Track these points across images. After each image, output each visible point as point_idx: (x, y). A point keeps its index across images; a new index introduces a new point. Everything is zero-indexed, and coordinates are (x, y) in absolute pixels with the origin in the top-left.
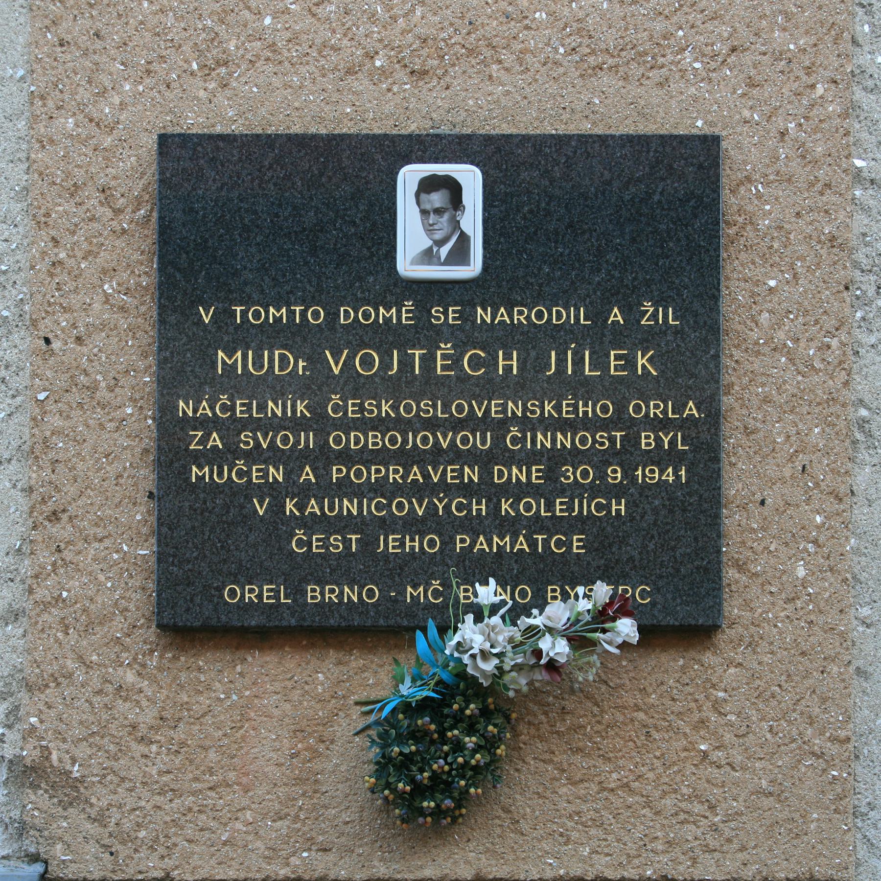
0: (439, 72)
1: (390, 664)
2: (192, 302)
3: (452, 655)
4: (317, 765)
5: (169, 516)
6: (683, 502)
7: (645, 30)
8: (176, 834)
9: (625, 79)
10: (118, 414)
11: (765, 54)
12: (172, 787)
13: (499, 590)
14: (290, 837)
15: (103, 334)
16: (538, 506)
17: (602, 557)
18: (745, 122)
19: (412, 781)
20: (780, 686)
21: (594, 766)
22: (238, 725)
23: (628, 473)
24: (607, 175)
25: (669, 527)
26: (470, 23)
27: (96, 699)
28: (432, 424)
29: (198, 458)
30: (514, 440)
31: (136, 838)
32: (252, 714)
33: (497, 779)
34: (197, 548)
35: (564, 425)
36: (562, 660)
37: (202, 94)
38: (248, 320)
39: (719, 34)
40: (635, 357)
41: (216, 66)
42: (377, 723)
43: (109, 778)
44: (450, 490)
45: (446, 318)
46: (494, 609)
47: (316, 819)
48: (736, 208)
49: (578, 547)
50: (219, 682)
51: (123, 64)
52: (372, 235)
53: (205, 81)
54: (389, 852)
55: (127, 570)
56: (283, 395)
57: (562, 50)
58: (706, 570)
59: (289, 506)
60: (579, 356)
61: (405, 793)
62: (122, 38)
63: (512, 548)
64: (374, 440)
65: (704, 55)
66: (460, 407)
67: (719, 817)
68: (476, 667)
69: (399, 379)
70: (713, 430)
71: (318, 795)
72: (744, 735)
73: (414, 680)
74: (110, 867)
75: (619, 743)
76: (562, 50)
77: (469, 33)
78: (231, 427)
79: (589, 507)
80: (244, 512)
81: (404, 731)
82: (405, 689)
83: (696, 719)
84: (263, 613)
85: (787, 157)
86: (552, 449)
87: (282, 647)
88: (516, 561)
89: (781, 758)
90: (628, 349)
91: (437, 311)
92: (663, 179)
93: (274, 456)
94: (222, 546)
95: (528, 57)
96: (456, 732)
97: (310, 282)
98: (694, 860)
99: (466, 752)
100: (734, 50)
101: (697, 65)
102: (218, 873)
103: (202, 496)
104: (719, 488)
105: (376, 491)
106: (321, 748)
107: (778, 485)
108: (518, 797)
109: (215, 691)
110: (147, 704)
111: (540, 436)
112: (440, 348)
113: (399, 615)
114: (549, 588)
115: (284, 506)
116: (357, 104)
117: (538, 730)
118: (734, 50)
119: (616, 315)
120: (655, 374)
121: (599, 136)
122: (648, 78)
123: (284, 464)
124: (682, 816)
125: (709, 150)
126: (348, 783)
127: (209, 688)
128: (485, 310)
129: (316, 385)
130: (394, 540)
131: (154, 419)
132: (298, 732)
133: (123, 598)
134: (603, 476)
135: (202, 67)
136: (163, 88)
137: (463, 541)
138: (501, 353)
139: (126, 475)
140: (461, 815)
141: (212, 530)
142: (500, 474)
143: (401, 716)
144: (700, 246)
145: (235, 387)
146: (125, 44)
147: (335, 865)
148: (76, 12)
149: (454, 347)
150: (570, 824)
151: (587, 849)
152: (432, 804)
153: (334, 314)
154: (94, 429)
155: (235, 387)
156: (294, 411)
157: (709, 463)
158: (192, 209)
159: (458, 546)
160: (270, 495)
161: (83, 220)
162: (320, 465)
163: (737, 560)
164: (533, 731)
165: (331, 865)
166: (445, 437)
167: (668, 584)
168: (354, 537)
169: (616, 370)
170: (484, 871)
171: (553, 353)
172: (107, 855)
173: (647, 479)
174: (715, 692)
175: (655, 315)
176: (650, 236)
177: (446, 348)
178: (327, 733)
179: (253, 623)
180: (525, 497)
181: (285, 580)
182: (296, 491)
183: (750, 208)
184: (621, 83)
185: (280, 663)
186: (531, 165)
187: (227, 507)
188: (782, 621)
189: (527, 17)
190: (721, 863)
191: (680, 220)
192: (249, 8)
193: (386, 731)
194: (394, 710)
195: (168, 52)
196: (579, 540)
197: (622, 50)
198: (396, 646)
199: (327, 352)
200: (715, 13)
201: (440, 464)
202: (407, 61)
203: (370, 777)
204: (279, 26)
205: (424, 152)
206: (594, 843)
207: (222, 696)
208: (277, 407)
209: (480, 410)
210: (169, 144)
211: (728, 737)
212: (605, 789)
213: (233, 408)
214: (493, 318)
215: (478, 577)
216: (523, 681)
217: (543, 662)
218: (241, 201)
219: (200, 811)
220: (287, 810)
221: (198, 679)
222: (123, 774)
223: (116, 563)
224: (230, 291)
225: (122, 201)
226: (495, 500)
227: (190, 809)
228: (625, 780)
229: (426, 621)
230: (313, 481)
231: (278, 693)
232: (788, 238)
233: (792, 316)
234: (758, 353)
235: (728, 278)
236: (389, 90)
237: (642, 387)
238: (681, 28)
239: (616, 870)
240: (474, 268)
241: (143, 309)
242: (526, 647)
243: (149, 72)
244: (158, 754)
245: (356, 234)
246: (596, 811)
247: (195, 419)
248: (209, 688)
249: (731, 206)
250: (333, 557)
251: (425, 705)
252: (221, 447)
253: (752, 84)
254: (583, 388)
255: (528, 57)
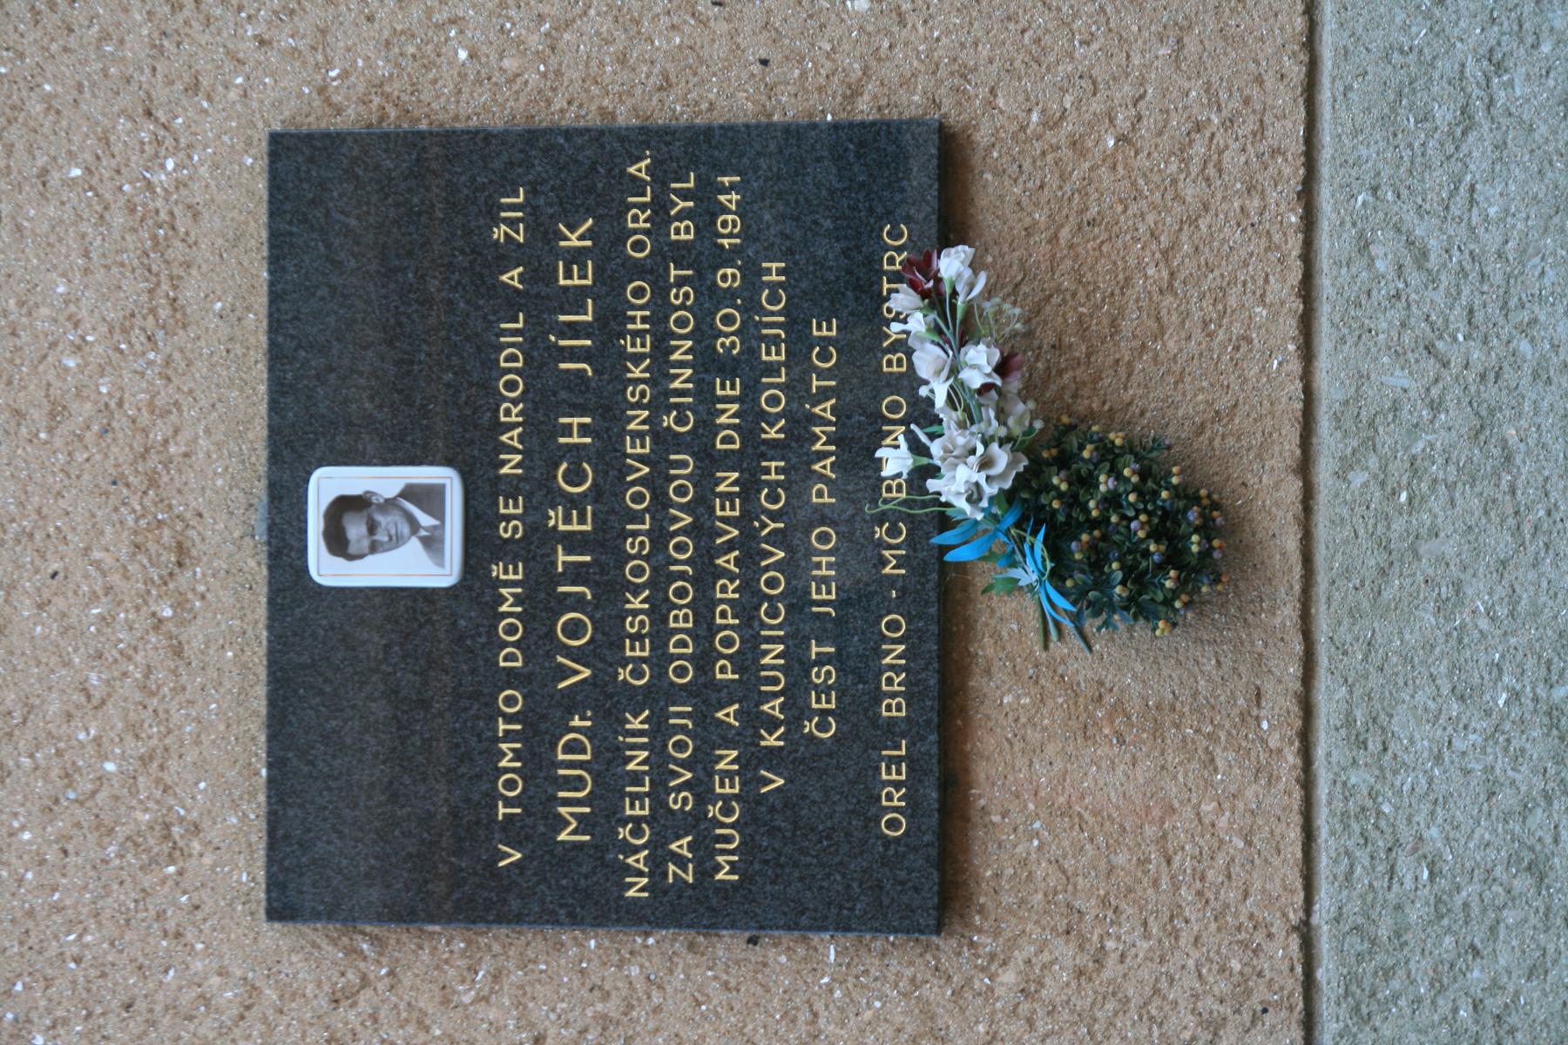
0: (179, 526)
1: (990, 599)
2: (493, 875)
3: (983, 510)
4: (1134, 707)
5: (785, 914)
6: (767, 179)
7: (123, 238)
8: (1236, 915)
9: (188, 265)
10: (640, 986)
11: (154, 69)
12: (1166, 919)
13: (888, 441)
14: (1240, 747)
15: (531, 1005)
16: (772, 386)
17: (844, 295)
18: (245, 95)
19: (1161, 568)
20: (1023, 32)
21: (1137, 300)
22: (1076, 820)
23: (726, 258)
24: (323, 292)
25: (801, 199)
26: (114, 483)
27: (1042, 1026)
28: (659, 537)
29: (706, 870)
30: (681, 421)
31: (1241, 973)
32: (1062, 799)
33: (1157, 444)
34: (829, 875)
35: (661, 349)
36: (997, 356)
37: (208, 860)
38: (517, 797)
39: (129, 133)
40: (568, 250)
41: (168, 840)
42: (1077, 619)
43: (1154, 1012)
44: (749, 512)
45: (514, 517)
46: (917, 448)
47: (1213, 708)
48: (361, 108)
49: (829, 329)
50: (1015, 847)
51: (166, 972)
52: (402, 621)
53: (190, 855)
54: (1262, 601)
55: (857, 977)
56: (618, 749)
57: (152, 355)
58: (861, 145)
59: (771, 741)
60: (566, 329)
61: (1178, 578)
62: (132, 972)
63: (829, 423)
64: (681, 619)
65: (156, 156)
66: (637, 498)
67: (1213, 117)
68: (1002, 476)
69: (597, 583)
70: (668, 138)
71: (1178, 705)
72: (1094, 83)
73: (1014, 565)
74: (1284, 1014)
75: (1103, 265)
76: (152, 355)
77: (128, 485)
78: (664, 824)
79: (774, 312)
80: (779, 806)
81: (1089, 579)
82: (1028, 575)
83: (1070, 153)
84: (920, 781)
85: (292, 36)
86: (693, 367)
87: (966, 756)
88: (849, 417)
89: (1127, 27)
90: (557, 260)
91: (506, 530)
92: (328, 213)
93: (702, 763)
94: (828, 838)
95: (161, 401)
96: (1092, 504)
97: (465, 709)
98: (1276, 152)
99: (1121, 489)
100: (149, 113)
101: (170, 164)
102: (1293, 854)
103: (757, 866)
104: (747, 126)
105: (751, 618)
106: (1110, 699)
107: (739, 40)
108: (1180, 413)
109: (1028, 854)
110: (1046, 953)
111: (676, 385)
112: (555, 527)
113: (923, 584)
114: (885, 369)
115: (771, 749)
116: (221, 641)
117: (1084, 383)
118: (149, 113)
119: (512, 277)
120: (590, 221)
121: (271, 302)
122: (187, 233)
123: (713, 749)
124: (1211, 171)
125: (289, 149)
126: (1161, 660)
127: (1024, 862)
128: (504, 463)
129: (607, 701)
130: (819, 591)
131: (647, 935)
132: (1086, 733)
133: (896, 986)
134: (731, 294)
135: (172, 860)
136: (199, 915)
137: (820, 494)
138: (562, 440)
139: (725, 977)
140: (1209, 496)
141: (802, 851)
142: (727, 441)
143: (1069, 583)
144: (418, 160)
145: (607, 816)
146: (140, 968)
147: (1280, 681)
148: (98, 1037)
149: (554, 508)
150: (1221, 336)
151: (1258, 310)
152: (1195, 538)
153: (508, 675)
154: (661, 1021)
155: (607, 816)
156: (641, 733)
157: (714, 143)
158: (367, 875)
159: (826, 500)
160: (756, 769)
161: (376, 1030)
162: (714, 697)
163: (845, 97)
164: (1086, 392)
165: (1280, 688)
166: (676, 519)
167: (880, 198)
168: (814, 650)
169: (585, 277)
170: (1289, 462)
171: (563, 366)
172: (1267, 1018)
173: (736, 231)
174: (1032, 127)
175: (512, 223)
176: (404, 230)
177: (555, 518)
178: (1089, 691)
179: (935, 795)
180: (759, 405)
181: (874, 748)
182: (750, 732)
183: (361, 88)
184: (194, 272)
185: (988, 759)
186: (309, 397)
187: (773, 831)
188: (931, 30)
189: (107, 405)
190: (1279, 112)
191: (382, 189)
192: (94, 793)
193: (1090, 604)
194: (1064, 593)
195: (151, 907)
196: (819, 328)
197: (150, 271)
198: (965, 590)
199: (561, 686)
200: (100, 140)
201: (713, 526)
202: (165, 573)
203: (1154, 630)
204: (118, 751)
205: (292, 548)
206: (1249, 300)
207: (1036, 843)
208: (635, 757)
209: (639, 470)
210: (283, 905)
211: (1096, 106)
212: (1170, 285)
213: (637, 820)
214: (515, 451)
215: (870, 472)
216: (1020, 407)
217: (999, 382)
218: (356, 805)
219: (1202, 879)
220: (1200, 751)
221: (1011, 878)
222: (1148, 991)
223: (848, 994)
224: (478, 822)
225: (350, 976)
226: (763, 448)
227: (1200, 893)
228: (1158, 255)
229: (932, 547)
230: (736, 706)
231: (1031, 762)
232: (403, 32)
233: (508, 25)
234: (558, 73)
235: (456, 118)
236: (203, 597)
237: (610, 238)
238: (120, 188)
239: (1289, 268)
240: (445, 477)
241: (496, 948)
242: (972, 404)
243: (178, 935)
244: (1118, 939)
245: (401, 644)
246: (1202, 297)
247: (651, 875)
248: (1024, 862)
249: (359, 114)
250: (842, 680)
251: (1055, 549)
252: (690, 838)
253: (194, 88)
254: (611, 323)
255: (161, 401)
